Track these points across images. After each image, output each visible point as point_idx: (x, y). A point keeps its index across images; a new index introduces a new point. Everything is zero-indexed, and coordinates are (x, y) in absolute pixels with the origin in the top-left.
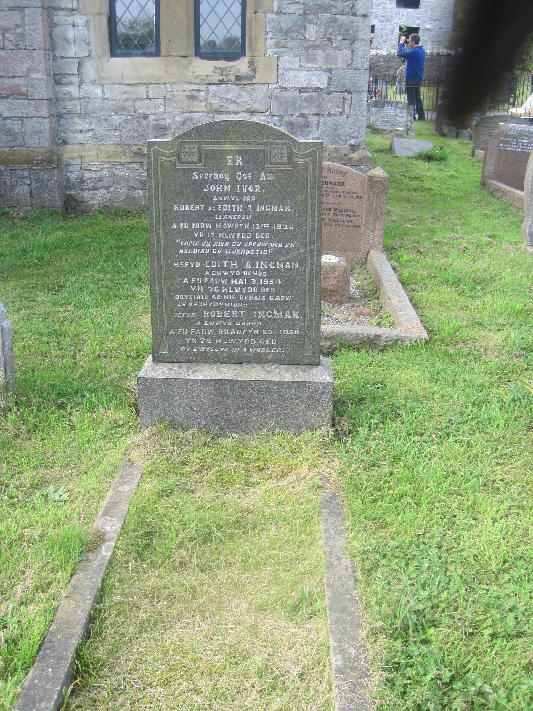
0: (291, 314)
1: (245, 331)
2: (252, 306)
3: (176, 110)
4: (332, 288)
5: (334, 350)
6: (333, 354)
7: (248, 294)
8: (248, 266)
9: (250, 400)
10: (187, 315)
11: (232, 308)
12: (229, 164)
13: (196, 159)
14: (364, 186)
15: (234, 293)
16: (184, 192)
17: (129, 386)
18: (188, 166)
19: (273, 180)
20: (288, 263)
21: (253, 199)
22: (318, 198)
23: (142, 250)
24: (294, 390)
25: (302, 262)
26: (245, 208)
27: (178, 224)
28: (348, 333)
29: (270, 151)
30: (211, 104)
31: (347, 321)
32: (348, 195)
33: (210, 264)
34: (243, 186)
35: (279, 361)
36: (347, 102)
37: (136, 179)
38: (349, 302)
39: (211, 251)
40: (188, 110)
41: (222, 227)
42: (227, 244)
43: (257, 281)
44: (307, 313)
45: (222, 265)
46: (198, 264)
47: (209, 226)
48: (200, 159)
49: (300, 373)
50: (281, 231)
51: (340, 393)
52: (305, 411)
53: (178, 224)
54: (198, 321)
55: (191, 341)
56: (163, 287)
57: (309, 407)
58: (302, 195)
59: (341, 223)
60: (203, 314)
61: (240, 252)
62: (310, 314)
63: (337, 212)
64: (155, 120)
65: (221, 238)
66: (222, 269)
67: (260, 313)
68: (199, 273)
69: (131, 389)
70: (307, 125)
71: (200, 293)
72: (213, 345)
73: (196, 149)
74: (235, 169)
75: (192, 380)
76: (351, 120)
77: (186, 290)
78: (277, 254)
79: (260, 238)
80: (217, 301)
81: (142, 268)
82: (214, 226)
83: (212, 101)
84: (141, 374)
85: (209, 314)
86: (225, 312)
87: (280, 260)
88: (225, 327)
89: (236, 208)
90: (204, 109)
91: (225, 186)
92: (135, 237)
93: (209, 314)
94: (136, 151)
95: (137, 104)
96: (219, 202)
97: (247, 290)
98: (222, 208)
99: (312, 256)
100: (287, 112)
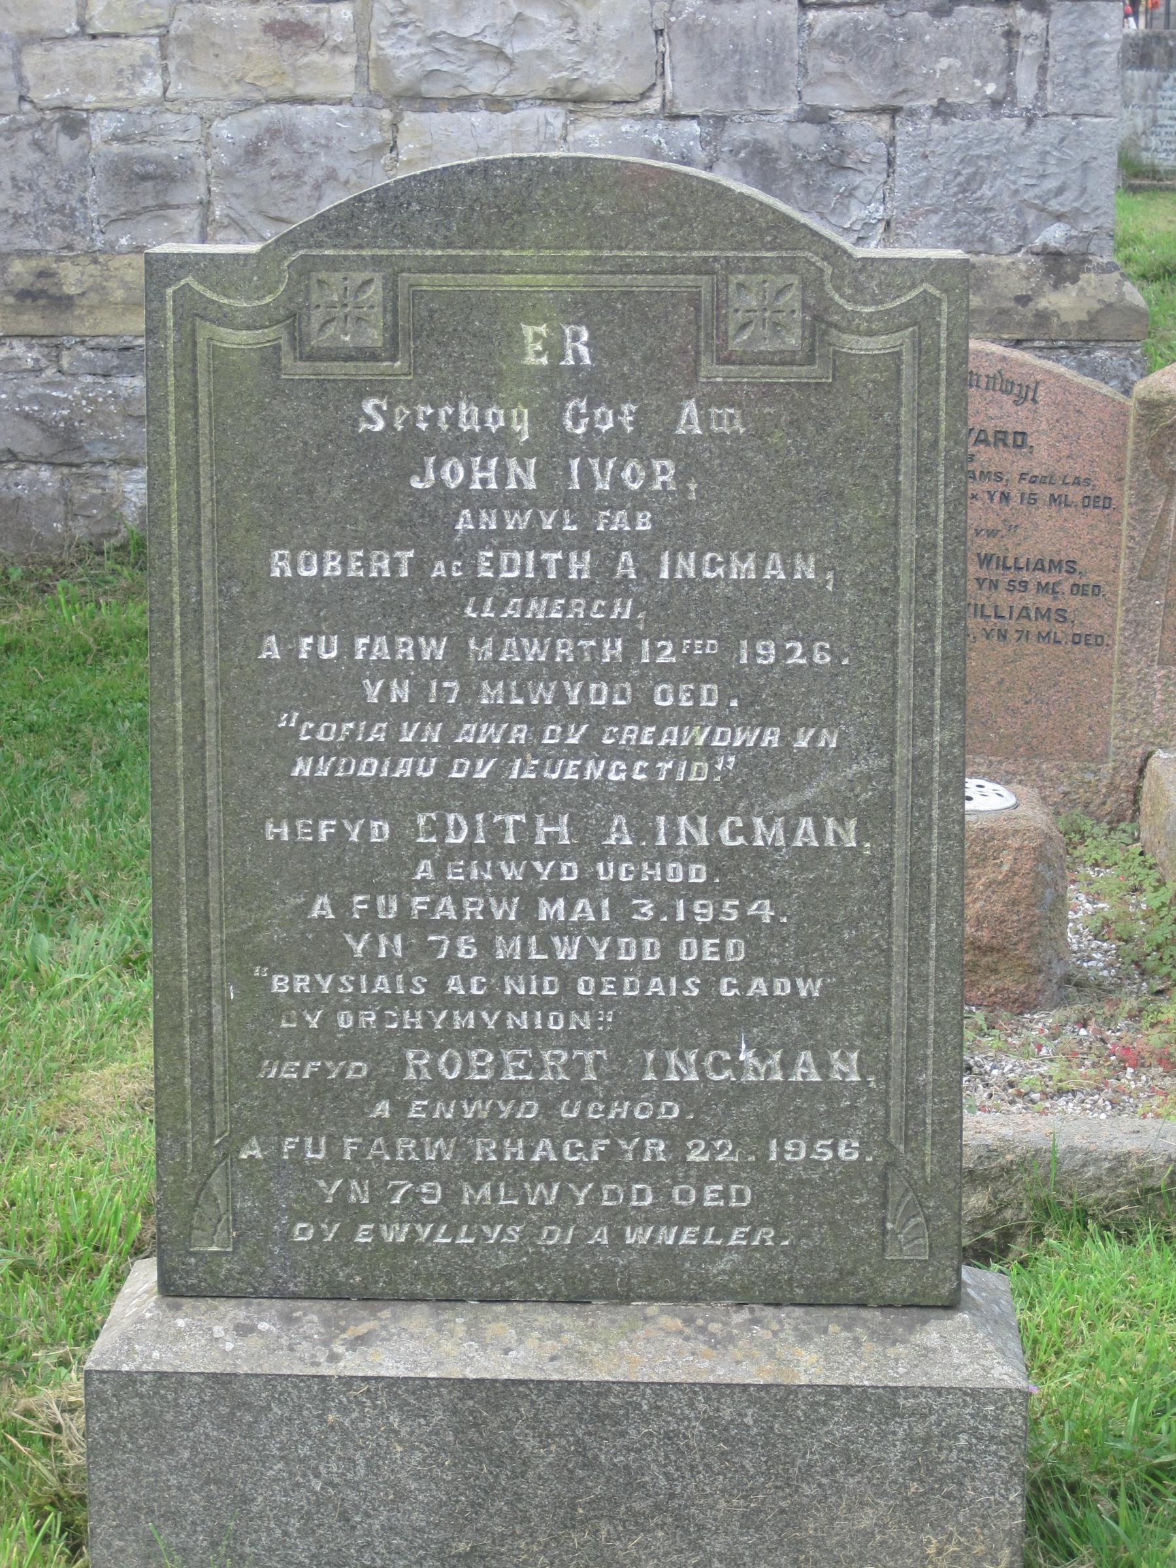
0: (824, 1066)
1: (600, 1145)
2: (635, 1029)
3: (219, 92)
4: (985, 935)
5: (1007, 1236)
6: (1004, 1251)
7: (617, 970)
8: (620, 836)
9: (631, 1480)
10: (325, 1071)
11: (538, 1038)
12: (531, 360)
13: (374, 337)
14: (1121, 448)
15: (552, 966)
16: (321, 490)
17: (28, 1413)
18: (338, 370)
19: (736, 436)
20: (806, 823)
21: (644, 524)
22: (950, 517)
23: (59, 756)
24: (839, 1428)
25: (874, 818)
26: (605, 566)
27: (288, 644)
28: (1072, 1150)
29: (720, 303)
30: (383, 64)
31: (1061, 1092)
32: (1044, 491)
33: (438, 828)
34: (595, 463)
35: (764, 1290)
36: (1028, 51)
37: (27, 417)
38: (1064, 1002)
39: (443, 768)
40: (276, 93)
41: (497, 653)
42: (520, 734)
43: (659, 910)
44: (896, 1056)
45: (495, 831)
46: (381, 831)
47: (435, 649)
48: (394, 340)
49: (868, 1347)
50: (777, 673)
51: (1054, 1443)
52: (892, 1531)
53: (288, 644)
54: (379, 1098)
55: (343, 1192)
56: (215, 936)
57: (912, 1512)
58: (874, 506)
59: (1011, 625)
60: (403, 1063)
61: (581, 770)
62: (913, 1060)
63: (994, 573)
64: (115, 138)
65: (493, 708)
66: (497, 850)
67: (672, 1057)
68: (387, 869)
69: (38, 1429)
70: (836, 162)
71: (390, 966)
72: (450, 1214)
73: (375, 292)
74: (556, 385)
75: (348, 1382)
76: (1045, 133)
77: (323, 950)
78: (754, 782)
79: (676, 707)
80: (472, 1003)
81: (67, 842)
82: (457, 650)
83: (388, 47)
84: (102, 1354)
85: (432, 1067)
86: (507, 1055)
87: (772, 806)
88: (506, 1129)
89: (563, 566)
90: (348, 88)
91: (513, 464)
92: (28, 693)
93: (432, 1067)
94: (26, 281)
95: (33, 59)
96: (481, 539)
97: (612, 950)
98: (495, 564)
99: (921, 790)
100: (742, 100)
